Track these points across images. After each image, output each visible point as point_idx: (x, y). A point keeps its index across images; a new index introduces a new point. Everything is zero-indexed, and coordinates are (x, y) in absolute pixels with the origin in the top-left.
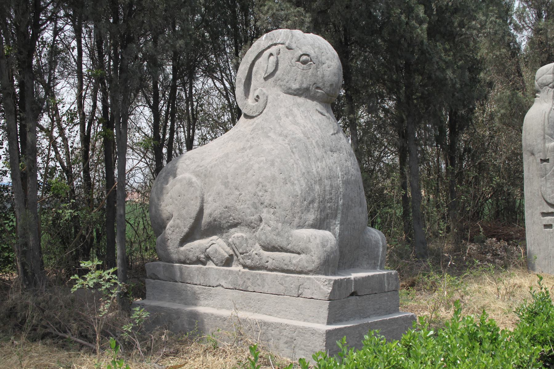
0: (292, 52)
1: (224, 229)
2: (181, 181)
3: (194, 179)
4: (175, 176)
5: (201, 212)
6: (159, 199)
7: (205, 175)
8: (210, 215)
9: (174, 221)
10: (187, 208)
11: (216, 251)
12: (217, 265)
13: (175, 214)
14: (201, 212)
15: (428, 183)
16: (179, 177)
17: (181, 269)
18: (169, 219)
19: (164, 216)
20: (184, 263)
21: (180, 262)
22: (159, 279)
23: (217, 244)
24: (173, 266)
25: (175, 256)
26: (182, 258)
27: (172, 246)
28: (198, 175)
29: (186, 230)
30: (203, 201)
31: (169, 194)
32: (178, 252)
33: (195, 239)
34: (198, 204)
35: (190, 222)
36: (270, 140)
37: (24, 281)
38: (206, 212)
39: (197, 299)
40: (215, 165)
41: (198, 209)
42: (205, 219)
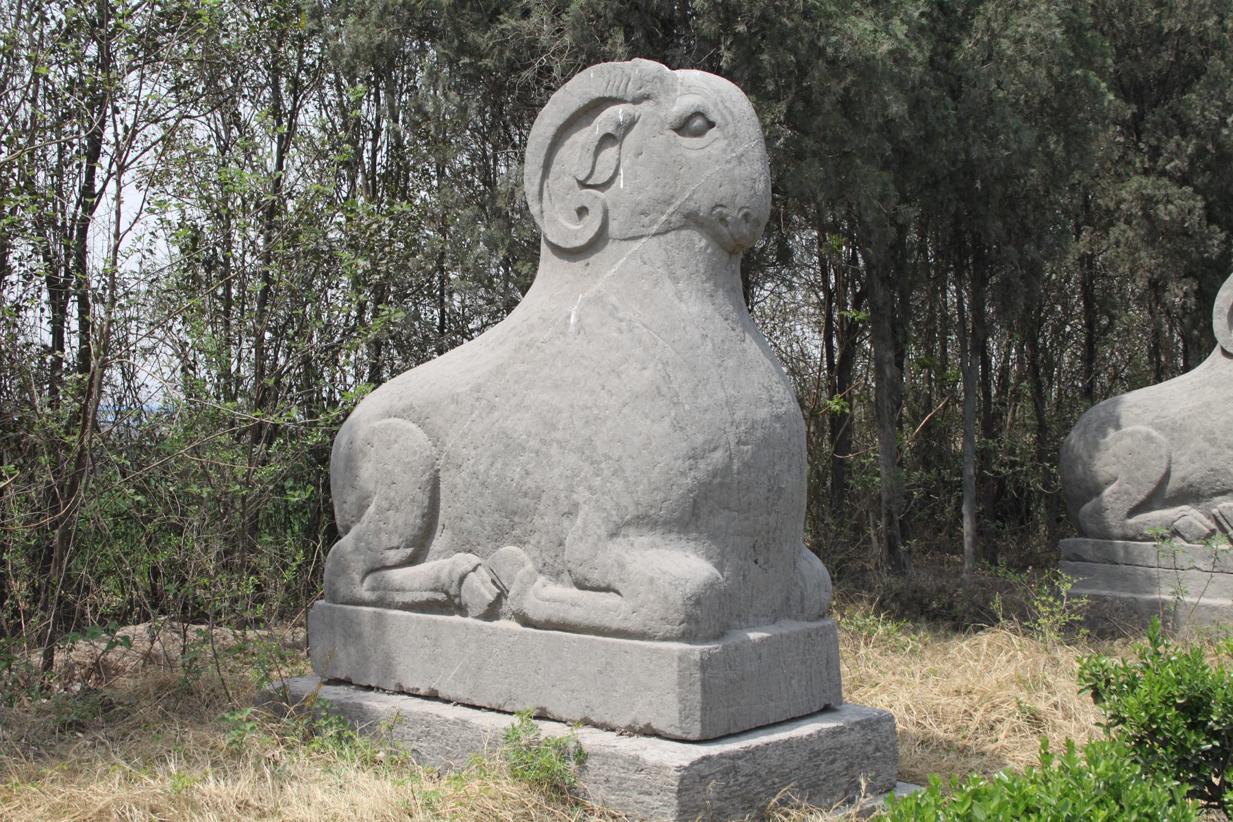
0: (668, 133)
1: (1203, 497)
2: (1131, 434)
3: (1155, 433)
4: (1118, 427)
5: (1167, 475)
6: (1091, 457)
7: (1173, 429)
8: (1183, 479)
9: (1120, 485)
10: (1143, 470)
11: (1191, 525)
12: (1189, 542)
13: (1122, 477)
14: (1167, 475)
15: (925, 480)
16: (1127, 429)
17: (1126, 548)
18: (1108, 483)
19: (1101, 479)
20: (1134, 539)
21: (1125, 538)
22: (1083, 560)
23: (1190, 516)
24: (1111, 544)
25: (1117, 531)
26: (1131, 533)
27: (1113, 519)
28: (1159, 428)
29: (1141, 497)
30: (1170, 462)
31: (1111, 451)
32: (1123, 526)
33: (1151, 509)
34: (1165, 465)
35: (1148, 488)
36: (608, 355)
37: (889, 560)
38: (1176, 475)
39: (1158, 585)
40: (1189, 417)
41: (1163, 471)
42: (1172, 485)
